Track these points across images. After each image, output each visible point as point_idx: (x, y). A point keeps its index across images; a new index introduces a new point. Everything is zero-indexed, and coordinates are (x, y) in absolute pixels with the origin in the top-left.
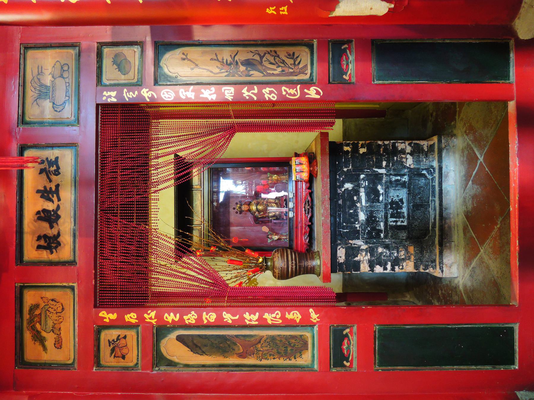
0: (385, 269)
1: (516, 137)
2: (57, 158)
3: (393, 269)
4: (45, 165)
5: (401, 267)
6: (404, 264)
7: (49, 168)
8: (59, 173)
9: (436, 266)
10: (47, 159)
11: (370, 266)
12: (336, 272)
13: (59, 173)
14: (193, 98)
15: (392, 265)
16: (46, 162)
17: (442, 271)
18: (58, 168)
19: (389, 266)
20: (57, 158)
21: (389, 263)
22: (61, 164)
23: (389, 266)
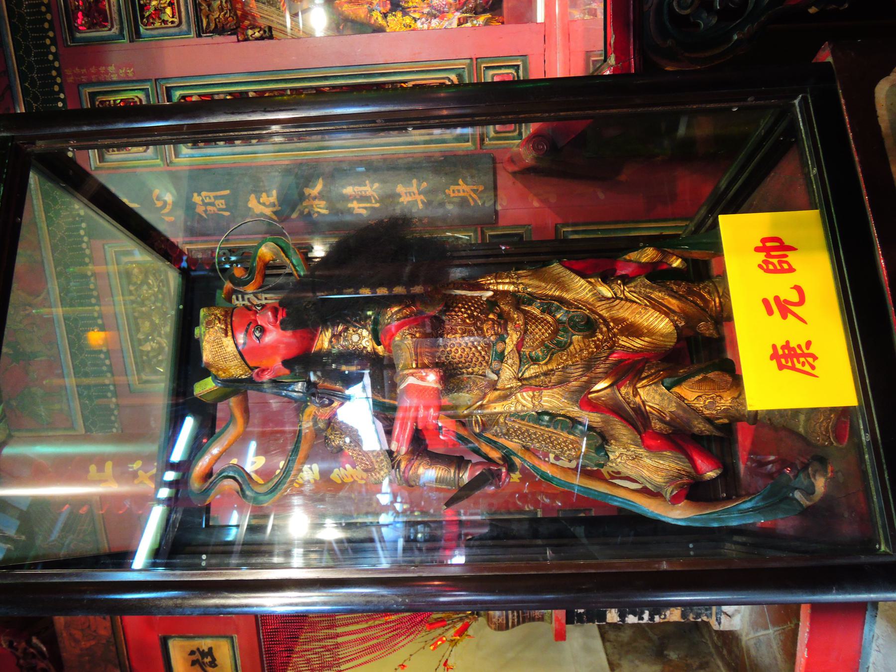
0: (641, 618)
1: (808, 624)
2: (210, 649)
3: (652, 618)
4: (197, 656)
5: (663, 617)
6: (668, 613)
7: (203, 659)
8: (216, 666)
9: (711, 614)
10: (198, 649)
11: (620, 616)
12: (572, 623)
13: (216, 666)
14: (363, 16)
15: (650, 615)
16: (197, 654)
17: (720, 623)
18: (214, 659)
19: (646, 616)
20: (210, 649)
21: (647, 612)
22: (216, 654)
23: (646, 616)
